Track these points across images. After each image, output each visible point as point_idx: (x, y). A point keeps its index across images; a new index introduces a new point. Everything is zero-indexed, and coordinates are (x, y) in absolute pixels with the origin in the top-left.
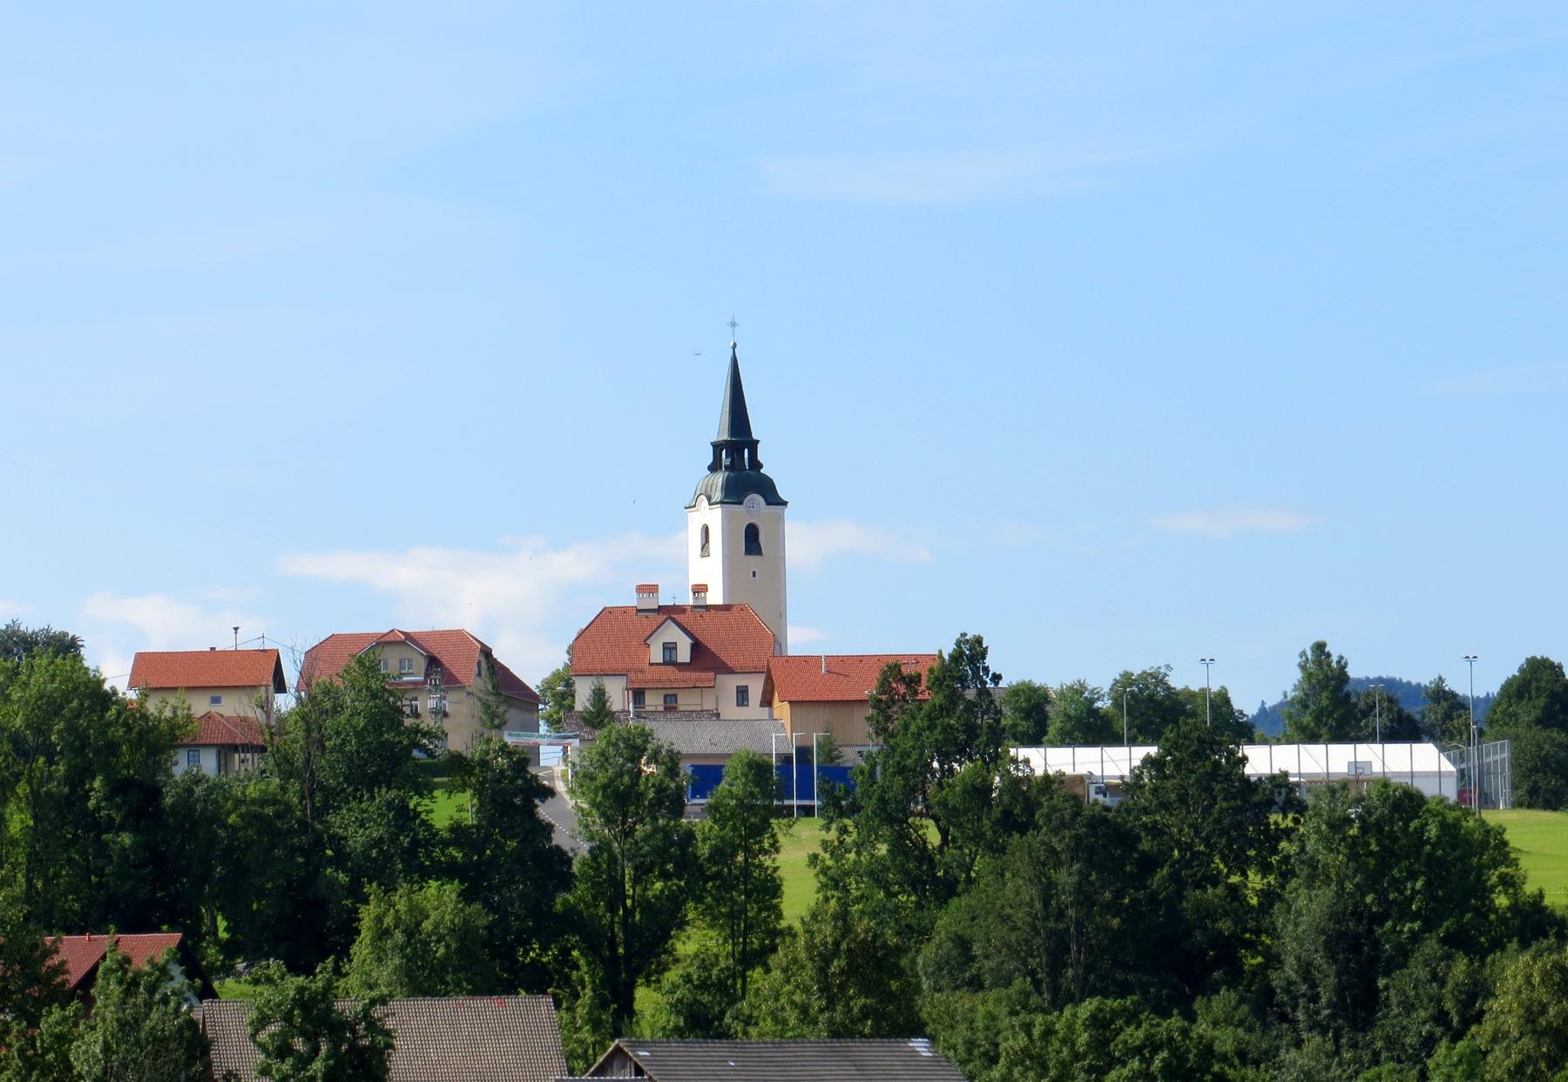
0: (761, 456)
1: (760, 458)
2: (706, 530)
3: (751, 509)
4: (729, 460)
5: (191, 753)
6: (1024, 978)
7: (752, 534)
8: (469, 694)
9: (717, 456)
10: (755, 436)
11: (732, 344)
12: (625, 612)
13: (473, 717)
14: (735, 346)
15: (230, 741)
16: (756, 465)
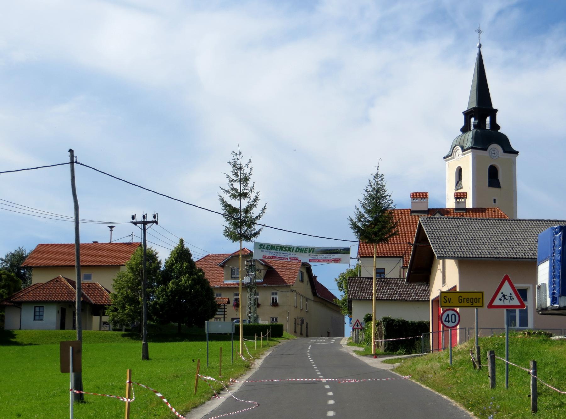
0: (499, 120)
1: (498, 122)
2: (459, 171)
3: (493, 155)
4: (477, 121)
5: (37, 309)
6: (118, 288)
7: (493, 173)
8: (292, 291)
9: (467, 121)
10: (494, 107)
11: (478, 45)
12: (402, 213)
13: (296, 307)
14: (480, 46)
15: (68, 299)
16: (494, 126)
